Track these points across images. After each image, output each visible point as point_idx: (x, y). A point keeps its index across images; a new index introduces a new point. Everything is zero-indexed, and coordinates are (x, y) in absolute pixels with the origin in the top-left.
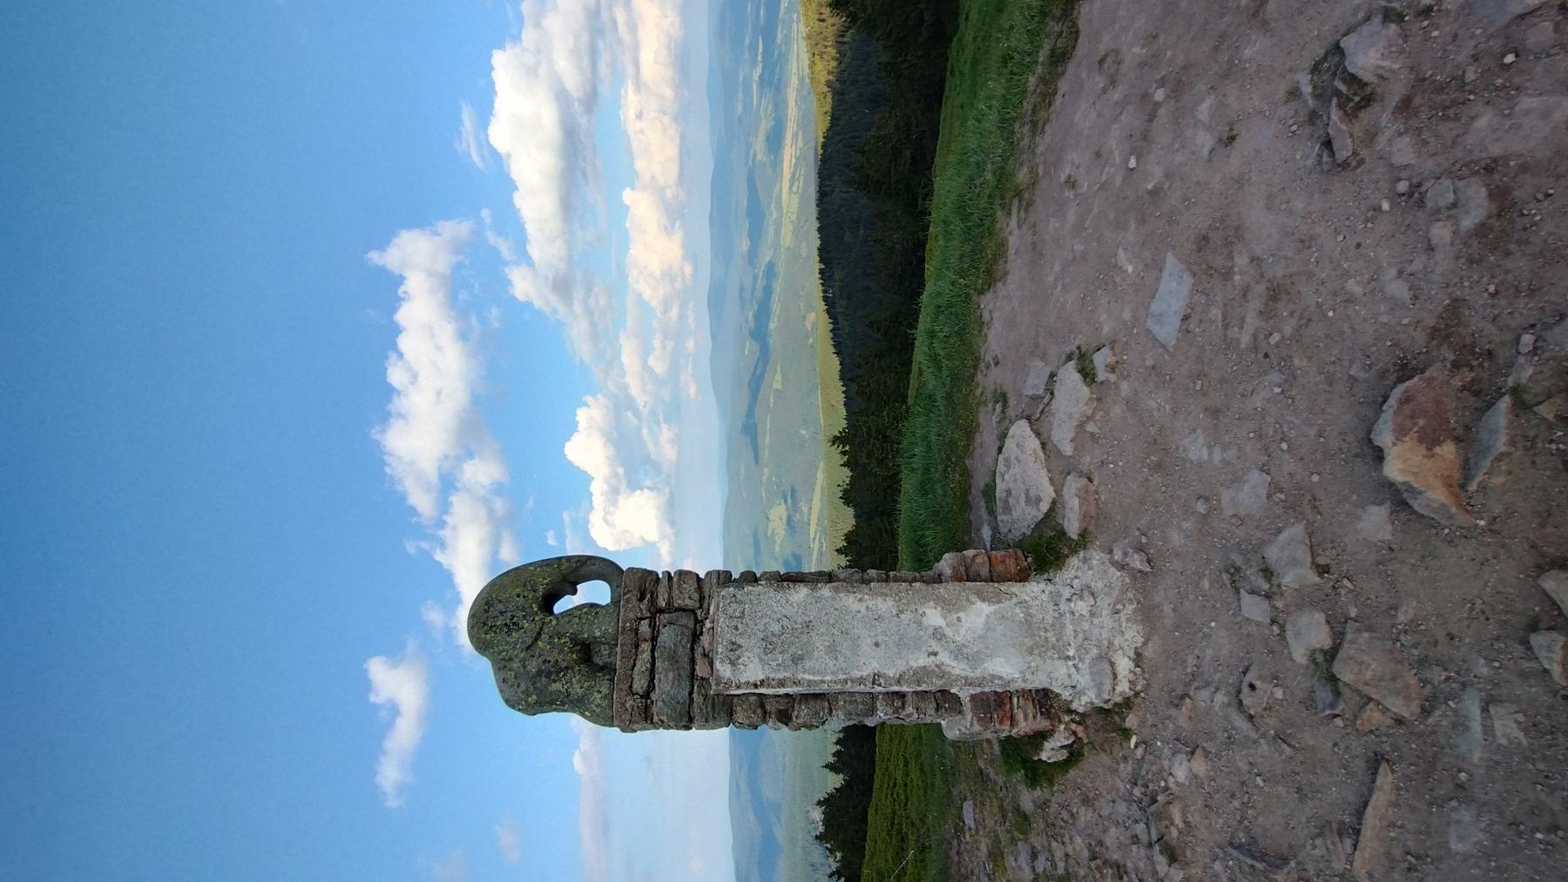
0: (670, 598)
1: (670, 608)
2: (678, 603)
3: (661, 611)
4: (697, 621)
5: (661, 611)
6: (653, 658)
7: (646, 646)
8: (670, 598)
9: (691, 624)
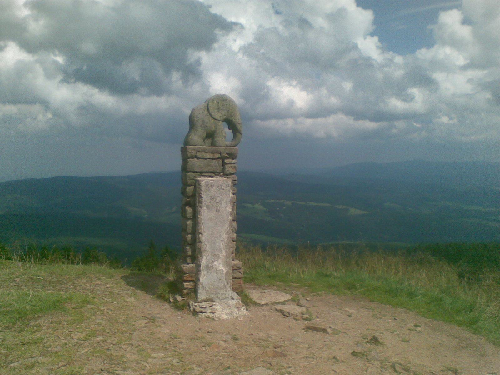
0: (227, 164)
1: (224, 164)
2: (226, 166)
3: (223, 161)
4: (219, 173)
5: (223, 161)
6: (208, 159)
7: (211, 156)
8: (227, 164)
9: (218, 171)
